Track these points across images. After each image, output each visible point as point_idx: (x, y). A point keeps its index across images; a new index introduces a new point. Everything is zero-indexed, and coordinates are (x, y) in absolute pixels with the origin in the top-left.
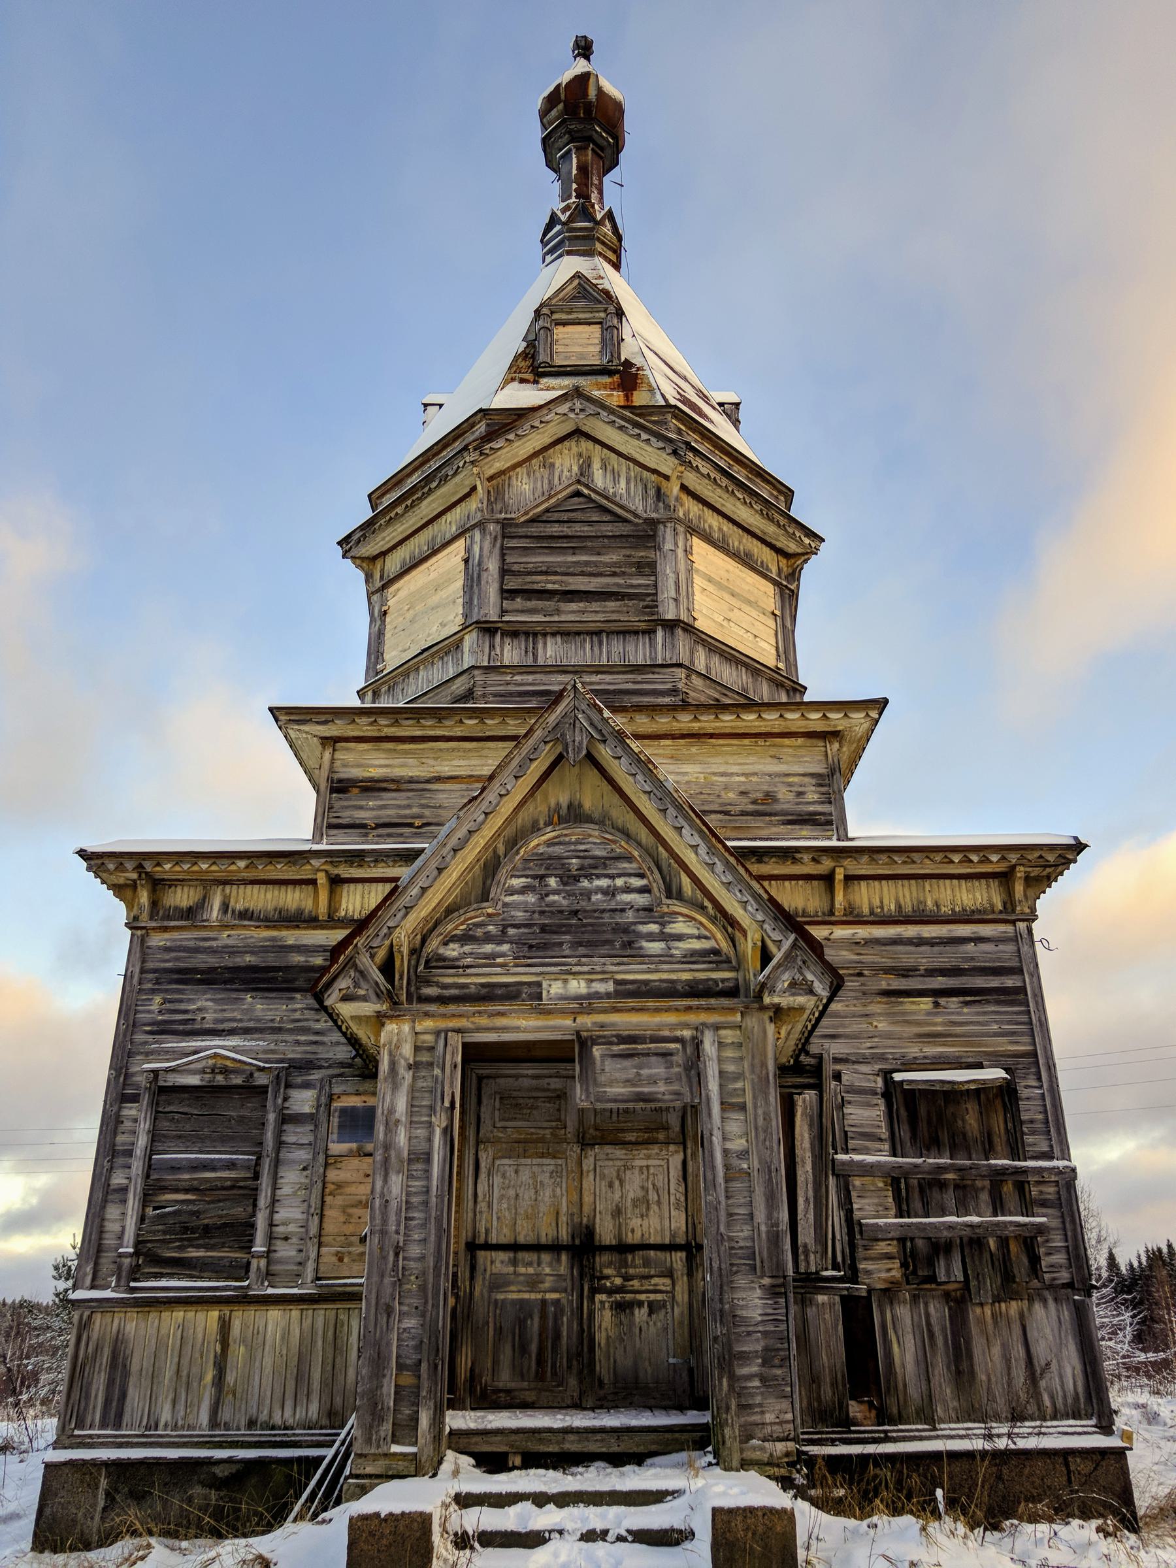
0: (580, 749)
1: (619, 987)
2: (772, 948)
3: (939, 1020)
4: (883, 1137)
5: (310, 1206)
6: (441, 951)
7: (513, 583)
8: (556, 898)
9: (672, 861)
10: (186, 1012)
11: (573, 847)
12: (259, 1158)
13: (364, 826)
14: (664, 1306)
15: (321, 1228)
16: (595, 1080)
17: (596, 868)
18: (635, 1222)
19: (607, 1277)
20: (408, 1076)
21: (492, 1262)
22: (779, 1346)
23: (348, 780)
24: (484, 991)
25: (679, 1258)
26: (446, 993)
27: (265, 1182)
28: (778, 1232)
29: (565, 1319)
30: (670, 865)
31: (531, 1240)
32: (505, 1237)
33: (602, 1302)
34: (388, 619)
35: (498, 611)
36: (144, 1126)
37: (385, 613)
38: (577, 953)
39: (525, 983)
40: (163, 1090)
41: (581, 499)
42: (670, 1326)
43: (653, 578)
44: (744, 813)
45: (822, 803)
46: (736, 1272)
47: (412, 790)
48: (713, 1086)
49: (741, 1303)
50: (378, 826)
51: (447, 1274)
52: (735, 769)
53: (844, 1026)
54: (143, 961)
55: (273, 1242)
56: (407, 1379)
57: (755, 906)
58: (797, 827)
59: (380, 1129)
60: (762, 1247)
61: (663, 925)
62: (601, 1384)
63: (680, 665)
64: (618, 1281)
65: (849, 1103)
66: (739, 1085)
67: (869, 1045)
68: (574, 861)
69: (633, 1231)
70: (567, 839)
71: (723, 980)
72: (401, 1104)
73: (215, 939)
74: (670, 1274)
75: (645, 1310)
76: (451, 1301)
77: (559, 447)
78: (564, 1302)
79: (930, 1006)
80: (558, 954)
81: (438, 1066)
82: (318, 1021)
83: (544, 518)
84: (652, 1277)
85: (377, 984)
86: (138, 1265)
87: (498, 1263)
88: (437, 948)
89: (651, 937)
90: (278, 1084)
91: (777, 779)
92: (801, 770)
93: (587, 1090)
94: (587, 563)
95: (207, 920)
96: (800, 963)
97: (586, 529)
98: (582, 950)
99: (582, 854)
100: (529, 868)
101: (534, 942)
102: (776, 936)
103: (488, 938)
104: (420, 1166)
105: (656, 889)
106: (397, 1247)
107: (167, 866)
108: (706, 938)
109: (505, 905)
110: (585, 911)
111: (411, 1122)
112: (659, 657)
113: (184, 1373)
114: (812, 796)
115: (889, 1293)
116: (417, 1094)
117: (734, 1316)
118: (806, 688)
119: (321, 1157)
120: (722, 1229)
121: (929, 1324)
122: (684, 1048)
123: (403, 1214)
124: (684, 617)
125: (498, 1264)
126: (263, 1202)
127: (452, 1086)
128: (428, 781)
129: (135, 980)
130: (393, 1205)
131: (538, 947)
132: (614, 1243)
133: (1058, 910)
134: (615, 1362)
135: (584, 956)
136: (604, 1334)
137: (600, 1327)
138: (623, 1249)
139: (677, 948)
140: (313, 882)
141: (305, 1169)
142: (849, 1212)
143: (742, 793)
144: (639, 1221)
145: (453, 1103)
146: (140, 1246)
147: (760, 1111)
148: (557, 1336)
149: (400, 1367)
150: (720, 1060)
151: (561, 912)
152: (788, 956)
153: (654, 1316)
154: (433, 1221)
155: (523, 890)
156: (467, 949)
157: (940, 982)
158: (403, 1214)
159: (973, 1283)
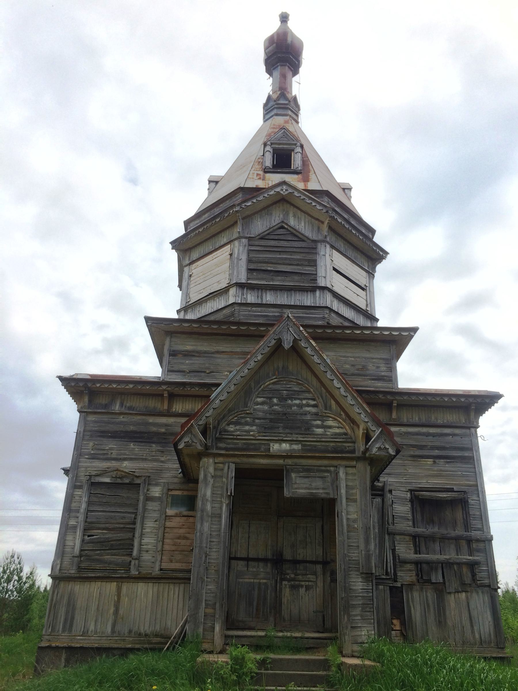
0: (289, 343)
2: (372, 434)
3: (436, 469)
5: (158, 537)
6: (227, 428)
7: (252, 267)
8: (277, 407)
9: (327, 394)
10: (104, 450)
11: (284, 386)
12: (136, 515)
13: (184, 372)
15: (163, 547)
17: (294, 395)
19: (288, 574)
20: (212, 481)
21: (237, 565)
22: (369, 603)
24: (245, 446)
26: (229, 446)
27: (138, 526)
29: (269, 591)
30: (326, 396)
31: (255, 556)
32: (244, 555)
33: (286, 585)
34: (192, 279)
35: (245, 278)
36: (85, 499)
37: (190, 276)
39: (263, 444)
40: (93, 484)
41: (284, 230)
43: (315, 267)
44: (353, 375)
45: (388, 372)
46: (352, 570)
47: (206, 357)
48: (343, 491)
50: (190, 372)
54: (85, 427)
56: (210, 611)
57: (365, 415)
58: (376, 382)
61: (323, 421)
62: (284, 620)
63: (327, 307)
64: (293, 576)
65: (395, 503)
66: (354, 491)
69: (299, 554)
71: (348, 446)
72: (209, 493)
73: (117, 419)
74: (315, 574)
75: (304, 589)
77: (274, 206)
79: (432, 463)
80: (278, 432)
83: (267, 237)
85: (201, 441)
86: (81, 561)
89: (318, 427)
90: (145, 483)
92: (379, 357)
94: (286, 259)
95: (114, 410)
96: (383, 441)
97: (285, 244)
98: (287, 431)
102: (373, 428)
103: (247, 424)
106: (206, 553)
107: (98, 385)
108: (341, 428)
109: (254, 409)
110: (289, 414)
111: (213, 500)
113: (101, 609)
115: (411, 586)
116: (215, 489)
117: (350, 589)
119: (164, 516)
120: (346, 552)
121: (427, 600)
122: (331, 474)
123: (209, 540)
124: (329, 286)
126: (137, 535)
127: (231, 486)
128: (213, 353)
129: (82, 434)
130: (205, 535)
133: (488, 423)
134: (291, 611)
135: (288, 433)
136: (286, 598)
137: (284, 595)
138: (295, 562)
139: (329, 432)
140: (162, 395)
141: (155, 521)
142: (394, 550)
143: (353, 365)
146: (82, 552)
149: (207, 606)
151: (279, 414)
152: (378, 437)
153: (308, 592)
154: (222, 543)
155: (262, 403)
156: (238, 427)
157: (436, 452)
159: (447, 584)
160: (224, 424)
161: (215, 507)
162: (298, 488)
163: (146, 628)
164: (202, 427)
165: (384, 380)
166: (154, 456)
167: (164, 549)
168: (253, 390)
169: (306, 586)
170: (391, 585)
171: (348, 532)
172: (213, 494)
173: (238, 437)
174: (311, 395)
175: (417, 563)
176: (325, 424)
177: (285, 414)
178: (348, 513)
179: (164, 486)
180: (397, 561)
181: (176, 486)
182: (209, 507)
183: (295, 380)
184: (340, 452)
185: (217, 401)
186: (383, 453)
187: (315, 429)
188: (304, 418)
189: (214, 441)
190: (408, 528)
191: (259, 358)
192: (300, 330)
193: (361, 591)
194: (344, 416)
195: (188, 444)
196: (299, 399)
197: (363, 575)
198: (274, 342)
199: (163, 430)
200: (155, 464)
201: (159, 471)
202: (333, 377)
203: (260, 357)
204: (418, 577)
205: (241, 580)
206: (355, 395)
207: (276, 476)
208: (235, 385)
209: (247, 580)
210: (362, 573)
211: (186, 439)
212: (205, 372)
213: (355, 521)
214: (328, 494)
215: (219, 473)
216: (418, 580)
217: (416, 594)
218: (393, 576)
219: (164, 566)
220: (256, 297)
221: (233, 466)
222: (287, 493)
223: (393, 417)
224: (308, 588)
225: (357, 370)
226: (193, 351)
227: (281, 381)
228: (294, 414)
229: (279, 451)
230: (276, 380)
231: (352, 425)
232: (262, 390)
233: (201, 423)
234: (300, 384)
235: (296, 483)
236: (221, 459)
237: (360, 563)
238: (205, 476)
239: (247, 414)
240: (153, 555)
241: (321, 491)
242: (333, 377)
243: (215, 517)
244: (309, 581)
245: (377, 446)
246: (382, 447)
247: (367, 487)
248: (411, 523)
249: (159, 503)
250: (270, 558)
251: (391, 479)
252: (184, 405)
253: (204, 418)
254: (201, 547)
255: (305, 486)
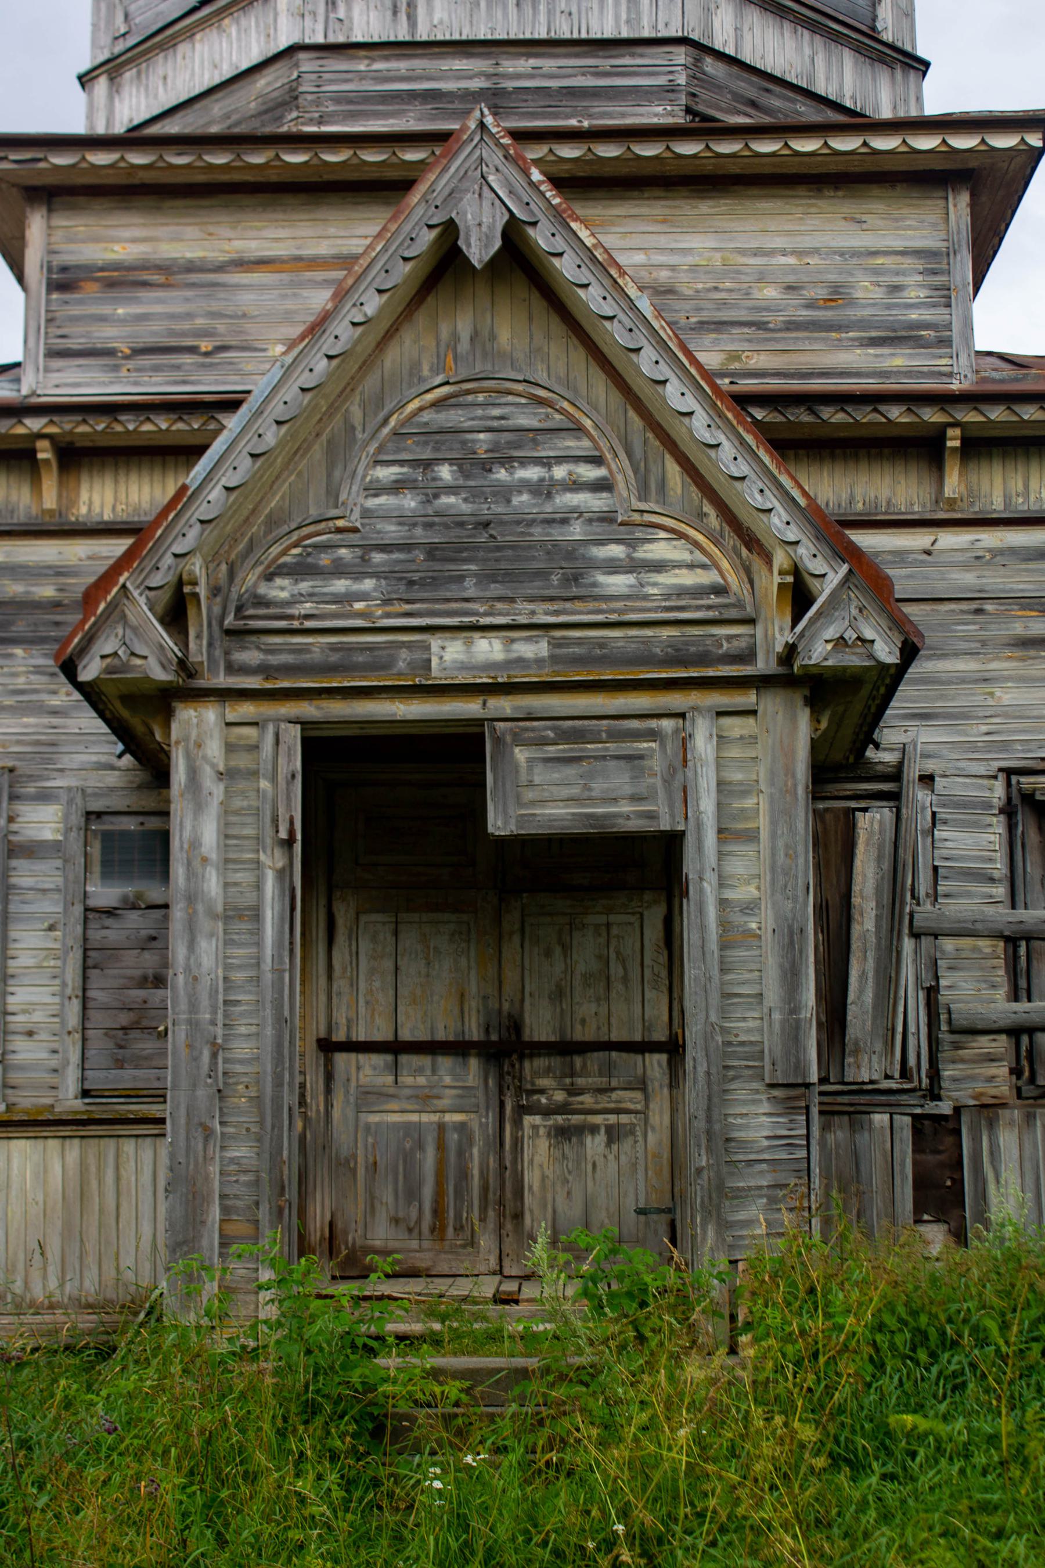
1: (558, 651)
2: (814, 584)
4: (997, 874)
5: (64, 985)
6: (263, 589)
8: (452, 499)
9: (650, 435)
13: (110, 353)
14: (632, 1133)
16: (518, 797)
17: (519, 446)
18: (587, 1009)
19: (542, 1091)
23: (78, 267)
24: (334, 658)
25: (656, 1064)
26: (274, 660)
28: (798, 1021)
32: (382, 1033)
33: (535, 1127)
38: (488, 594)
42: (641, 1161)
44: (792, 326)
45: (935, 305)
46: (734, 1078)
47: (193, 285)
48: (707, 804)
49: (739, 1121)
51: (291, 1084)
52: (779, 242)
53: (942, 697)
55: (10, 1038)
57: (785, 517)
58: (886, 351)
59: (178, 871)
60: (772, 1043)
61: (632, 544)
64: (559, 1096)
66: (749, 803)
67: (984, 728)
68: (482, 436)
69: (583, 1022)
70: (470, 398)
71: (729, 638)
72: (209, 834)
74: (642, 1085)
75: (601, 1138)
76: (299, 1125)
78: (475, 1126)
81: (265, 777)
82: (55, 692)
84: (614, 1089)
87: (370, 1070)
88: (255, 585)
89: (613, 567)
91: (855, 261)
92: (898, 244)
93: (505, 812)
96: (854, 612)
98: (496, 589)
99: (495, 424)
100: (405, 449)
101: (416, 577)
103: (339, 570)
104: (245, 926)
105: (621, 485)
106: (214, 1044)
108: (704, 567)
109: (366, 513)
110: (502, 523)
111: (227, 861)
112: (645, 22)
114: (916, 293)
115: (989, 1110)
116: (233, 819)
117: (728, 1140)
118: (927, 65)
119: (78, 910)
120: (713, 1018)
122: (663, 745)
125: (368, 1071)
130: (206, 982)
131: (422, 583)
132: (553, 1039)
134: (554, 1211)
135: (500, 599)
136: (537, 1173)
138: (566, 1049)
139: (655, 584)
140: (29, 454)
142: (932, 993)
143: (790, 288)
144: (593, 1008)
145: (291, 832)
147: (780, 843)
148: (464, 1175)
150: (720, 763)
151: (461, 524)
152: (834, 597)
153: (615, 1147)
154: (268, 1005)
155: (397, 487)
156: (305, 586)
158: (221, 998)
160: (252, 578)
161: (236, 884)
162: (543, 802)
163: (53, 1284)
164: (165, 597)
165: (918, 343)
166: (22, 692)
167: (88, 1026)
168: (359, 436)
169: (609, 1129)
170: (918, 1111)
171: (724, 946)
172: (227, 836)
173: (309, 624)
174: (586, 443)
175: (1014, 1032)
176: (635, 555)
177: (487, 525)
178: (722, 883)
179: (70, 802)
180: (944, 1027)
181: (118, 803)
182: (212, 884)
183: (519, 387)
184: (693, 669)
185: (216, 494)
186: (853, 660)
187: (602, 578)
188: (557, 534)
189: (217, 644)
190: (990, 910)
191: (370, 310)
192: (531, 183)
193: (766, 1143)
194: (713, 520)
195: (116, 661)
196: (538, 461)
197: (776, 1092)
198: (428, 237)
199: (47, 591)
200: (31, 720)
201: (47, 750)
202: (664, 371)
203: (372, 304)
204: (1019, 1078)
205: (374, 1118)
206: (749, 438)
207: (456, 756)
208: (279, 423)
209: (392, 1117)
210: (772, 1086)
211: (107, 645)
212: (193, 350)
213: (750, 907)
214: (651, 816)
215: (243, 761)
216: (1019, 1090)
217: (1008, 1139)
218: (925, 1082)
219: (97, 1080)
220: (389, 13)
221: (294, 733)
222: (499, 822)
223: (948, 492)
224: (614, 1135)
225: (808, 307)
226: (144, 266)
227: (468, 392)
228: (518, 523)
229: (464, 667)
230: (446, 390)
231: (745, 552)
232: (395, 433)
233: (156, 580)
234: (541, 402)
235: (531, 784)
236: (247, 710)
237: (766, 1051)
238: (193, 773)
239: (339, 530)
240: (55, 1046)
241: (625, 808)
242: (664, 371)
243: (241, 917)
244: (618, 1111)
245: (831, 632)
246: (850, 635)
247: (795, 786)
248: (1000, 891)
249: (59, 863)
250: (475, 1038)
251: (927, 736)
252: (122, 488)
253: (168, 560)
254: (193, 1024)
255: (566, 792)
